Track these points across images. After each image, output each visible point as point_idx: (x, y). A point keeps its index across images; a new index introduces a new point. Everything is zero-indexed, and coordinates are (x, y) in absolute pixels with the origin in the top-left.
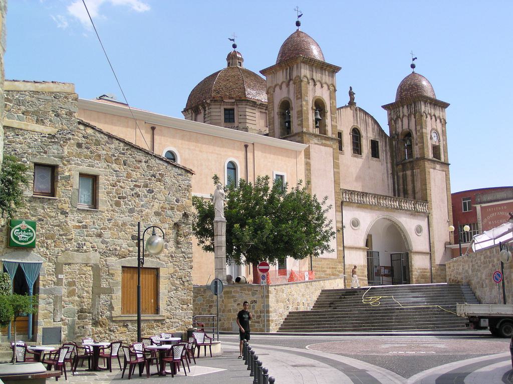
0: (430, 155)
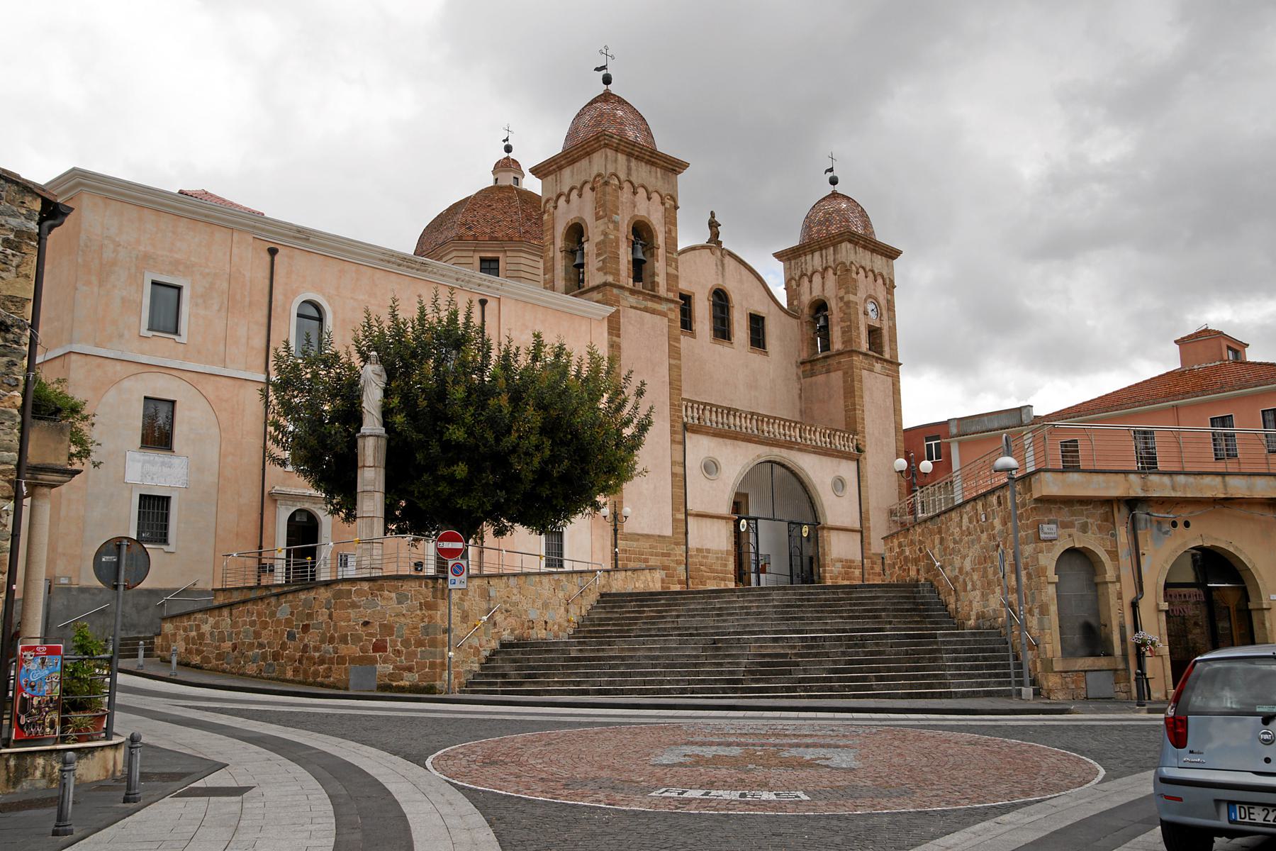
0: (864, 346)
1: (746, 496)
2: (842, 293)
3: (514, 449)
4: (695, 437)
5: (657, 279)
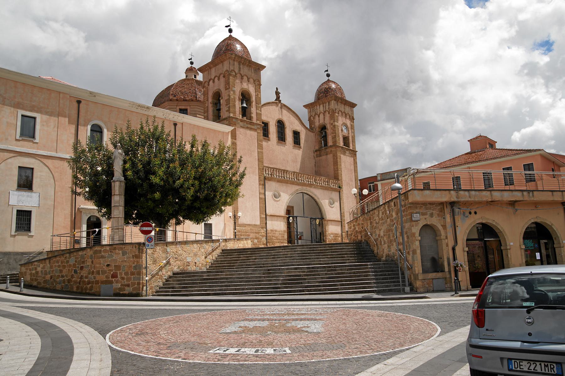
0: (342, 144)
1: (293, 207)
2: (332, 122)
3: (182, 186)
4: (269, 182)
5: (252, 115)
